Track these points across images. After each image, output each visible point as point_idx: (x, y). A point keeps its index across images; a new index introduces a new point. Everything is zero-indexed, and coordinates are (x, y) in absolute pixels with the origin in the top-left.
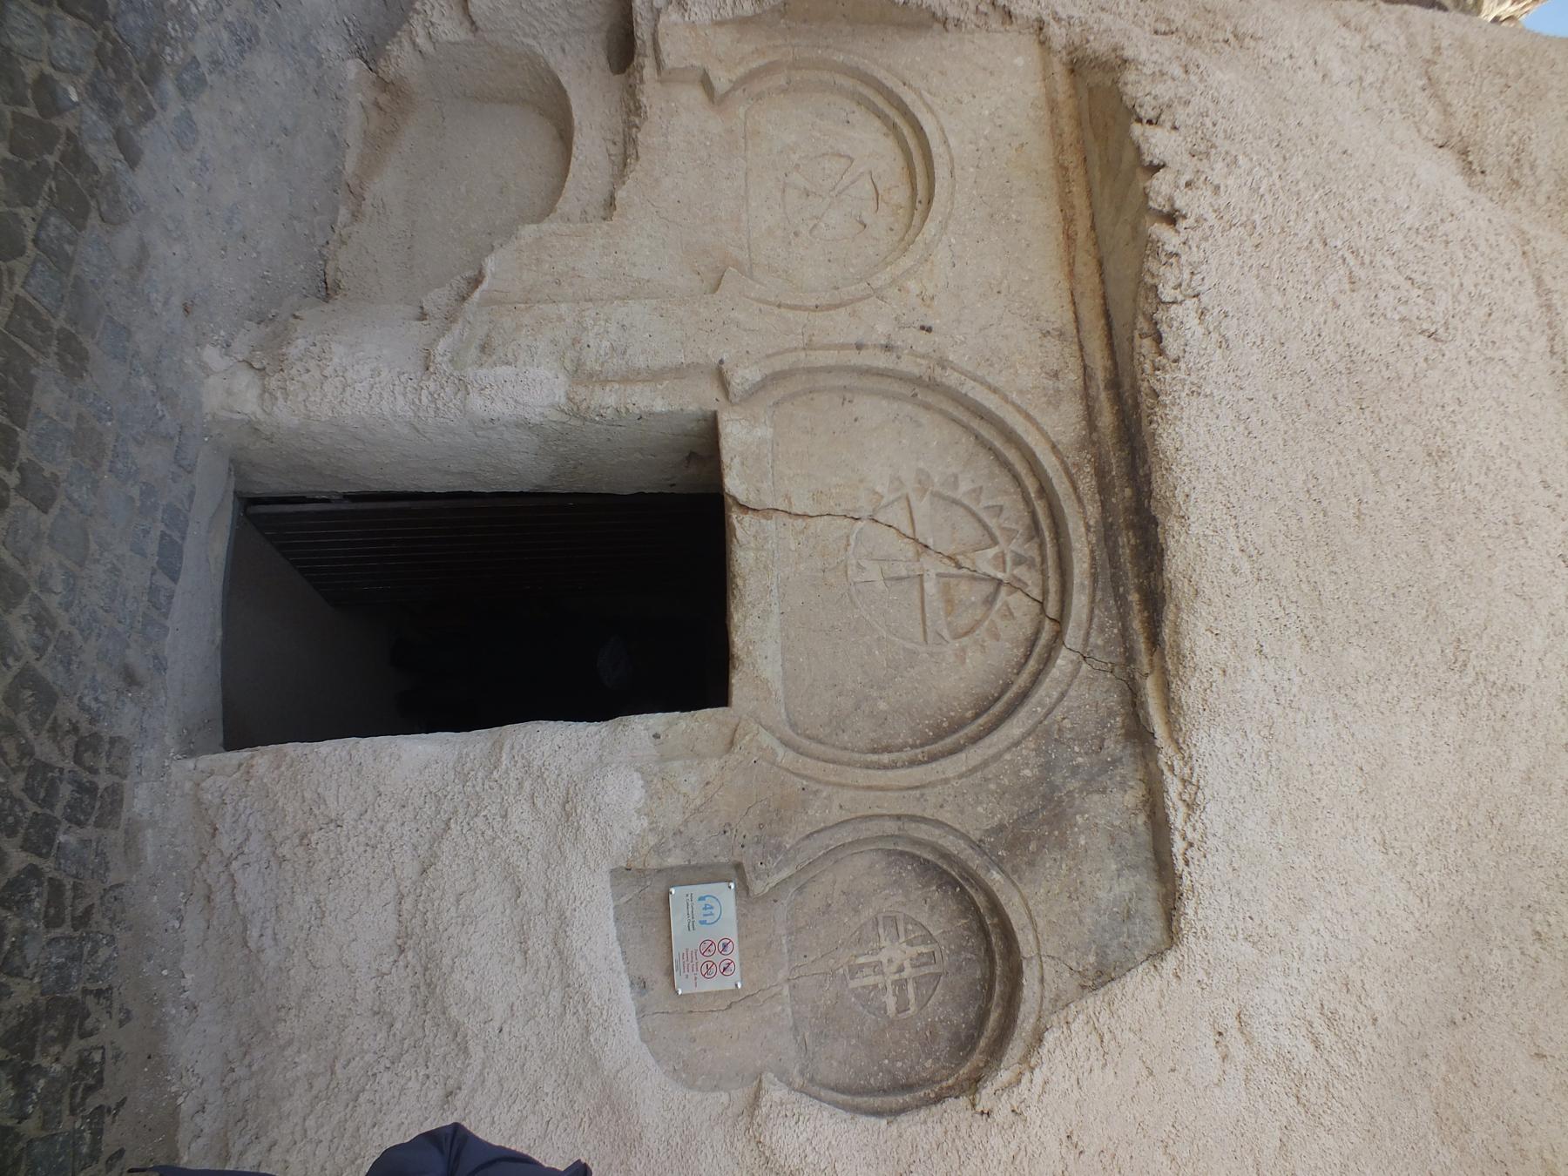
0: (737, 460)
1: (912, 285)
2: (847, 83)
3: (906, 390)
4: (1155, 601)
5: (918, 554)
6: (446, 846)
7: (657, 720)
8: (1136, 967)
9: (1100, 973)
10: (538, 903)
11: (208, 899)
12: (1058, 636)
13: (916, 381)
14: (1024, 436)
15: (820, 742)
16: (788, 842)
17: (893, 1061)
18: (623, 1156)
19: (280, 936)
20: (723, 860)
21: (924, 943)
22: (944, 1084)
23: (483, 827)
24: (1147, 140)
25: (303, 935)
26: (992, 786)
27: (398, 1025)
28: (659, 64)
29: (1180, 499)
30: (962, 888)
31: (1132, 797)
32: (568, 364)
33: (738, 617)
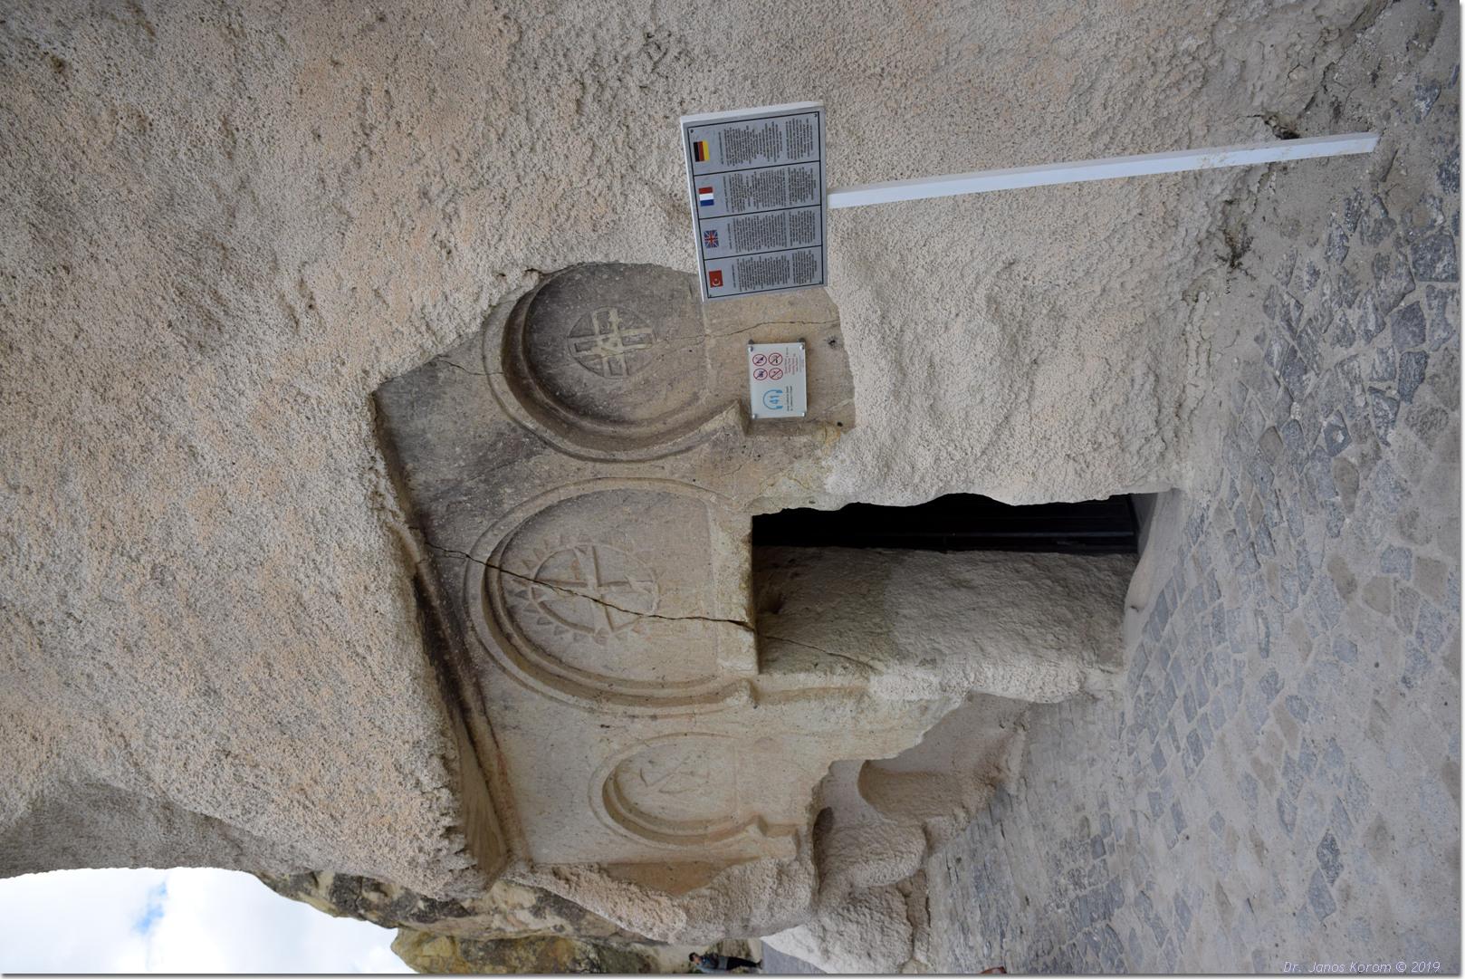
3: (615, 688)
6: (986, 439)
13: (611, 696)
16: (706, 447)
20: (761, 438)
21: (585, 357)
31: (419, 479)
33: (747, 566)
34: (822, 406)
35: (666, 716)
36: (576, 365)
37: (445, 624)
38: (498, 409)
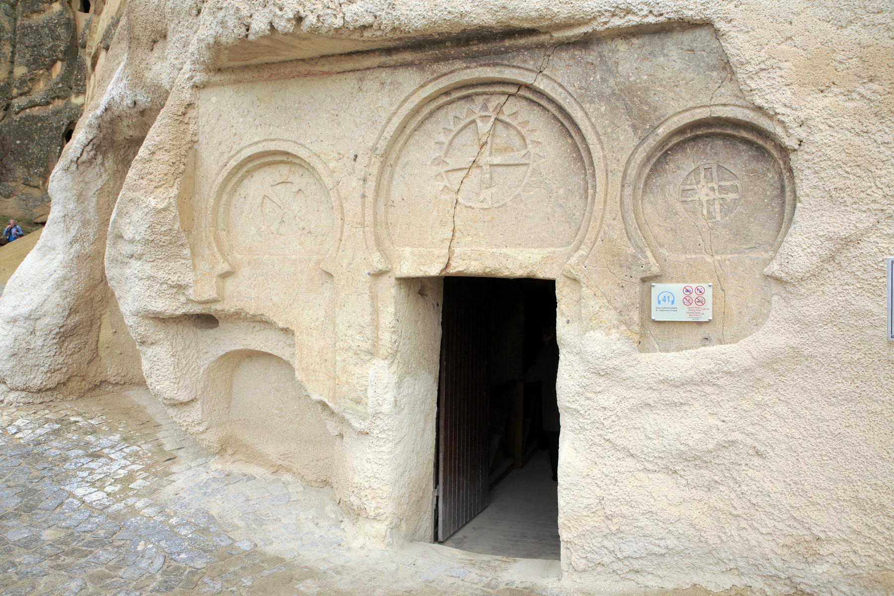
0: (422, 268)
1: (332, 165)
2: (225, 197)
3: (388, 169)
4: (510, 33)
5: (478, 167)
6: (619, 442)
7: (560, 321)
8: (722, 46)
9: (724, 68)
10: (655, 395)
11: (637, 572)
12: (528, 87)
13: (383, 165)
14: (415, 103)
15: (579, 229)
16: (631, 250)
17: (766, 196)
18: (802, 359)
19: (660, 536)
20: (638, 289)
22: (782, 167)
23: (610, 421)
24: (257, 33)
25: (661, 524)
26: (609, 130)
27: (716, 478)
28: (215, 301)
29: (450, 17)
30: (669, 150)
31: (622, 46)
32: (368, 358)
33: (506, 273)
34: (654, 330)
35: (363, 205)
36: (694, 167)
37: (482, 47)
38: (679, 110)
